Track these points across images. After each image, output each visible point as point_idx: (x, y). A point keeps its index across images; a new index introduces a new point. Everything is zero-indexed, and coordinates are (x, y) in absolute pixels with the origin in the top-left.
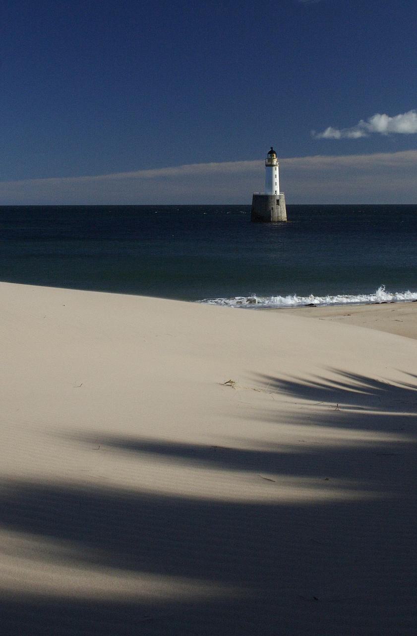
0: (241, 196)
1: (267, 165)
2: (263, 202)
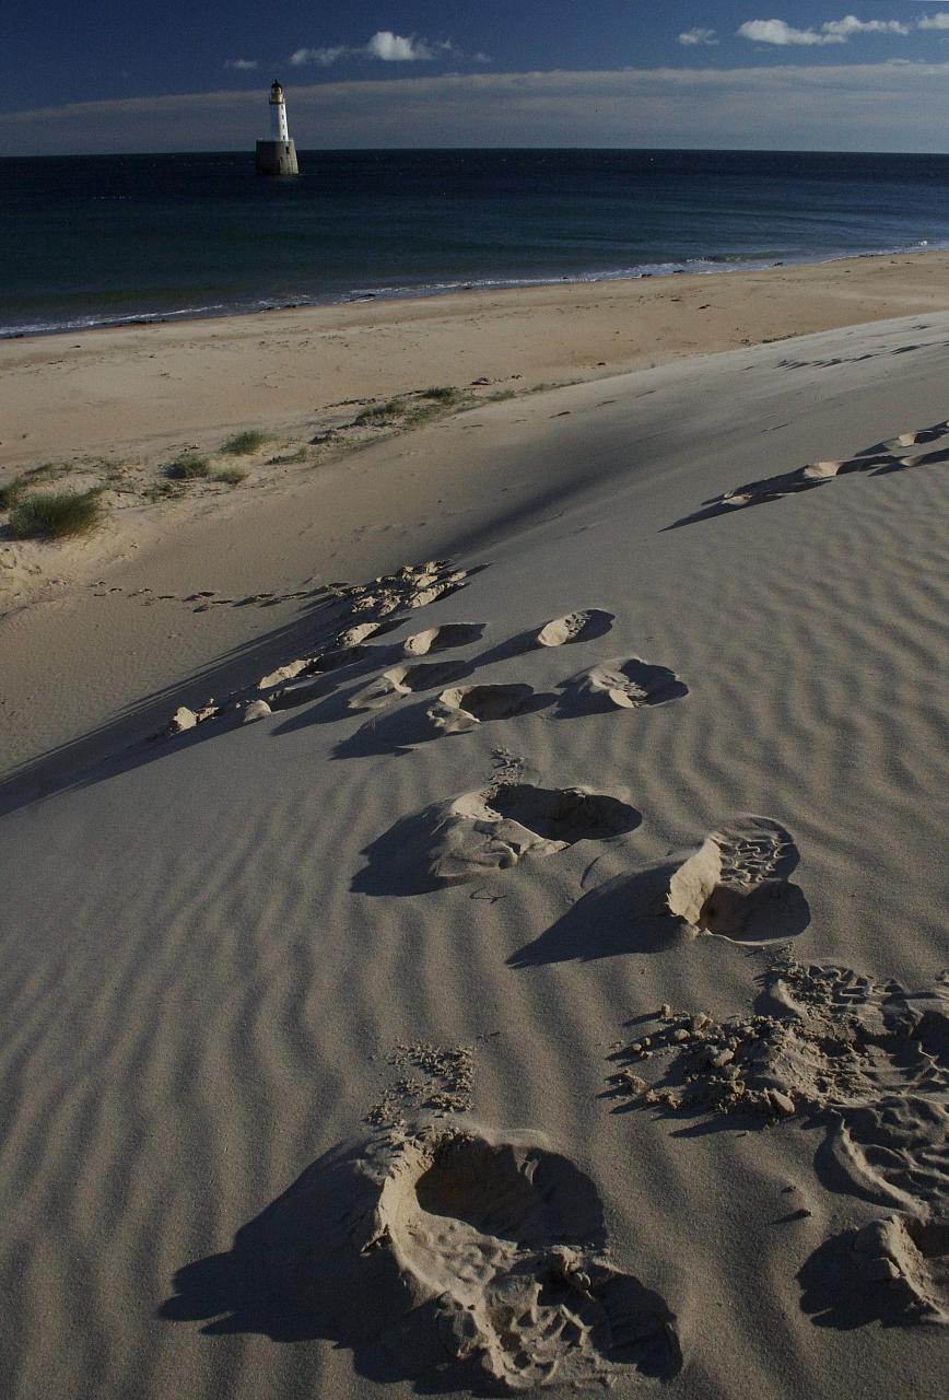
0: (240, 139)
1: (271, 103)
2: (270, 149)
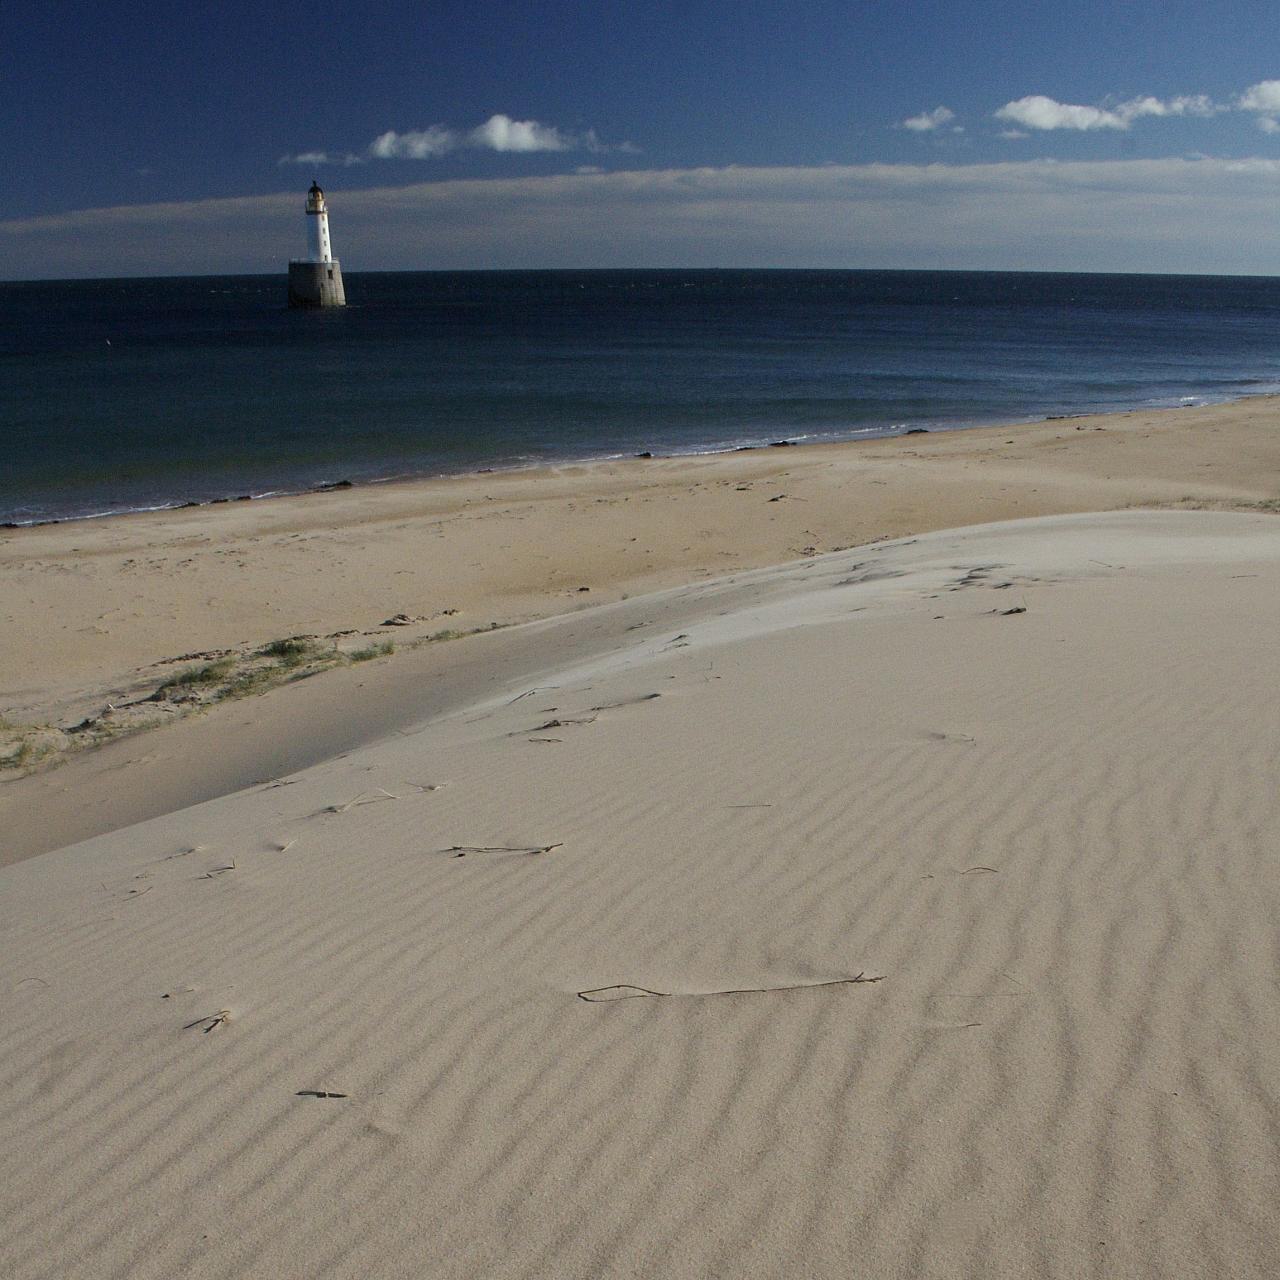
0: (270, 259)
1: (308, 213)
2: (307, 273)
